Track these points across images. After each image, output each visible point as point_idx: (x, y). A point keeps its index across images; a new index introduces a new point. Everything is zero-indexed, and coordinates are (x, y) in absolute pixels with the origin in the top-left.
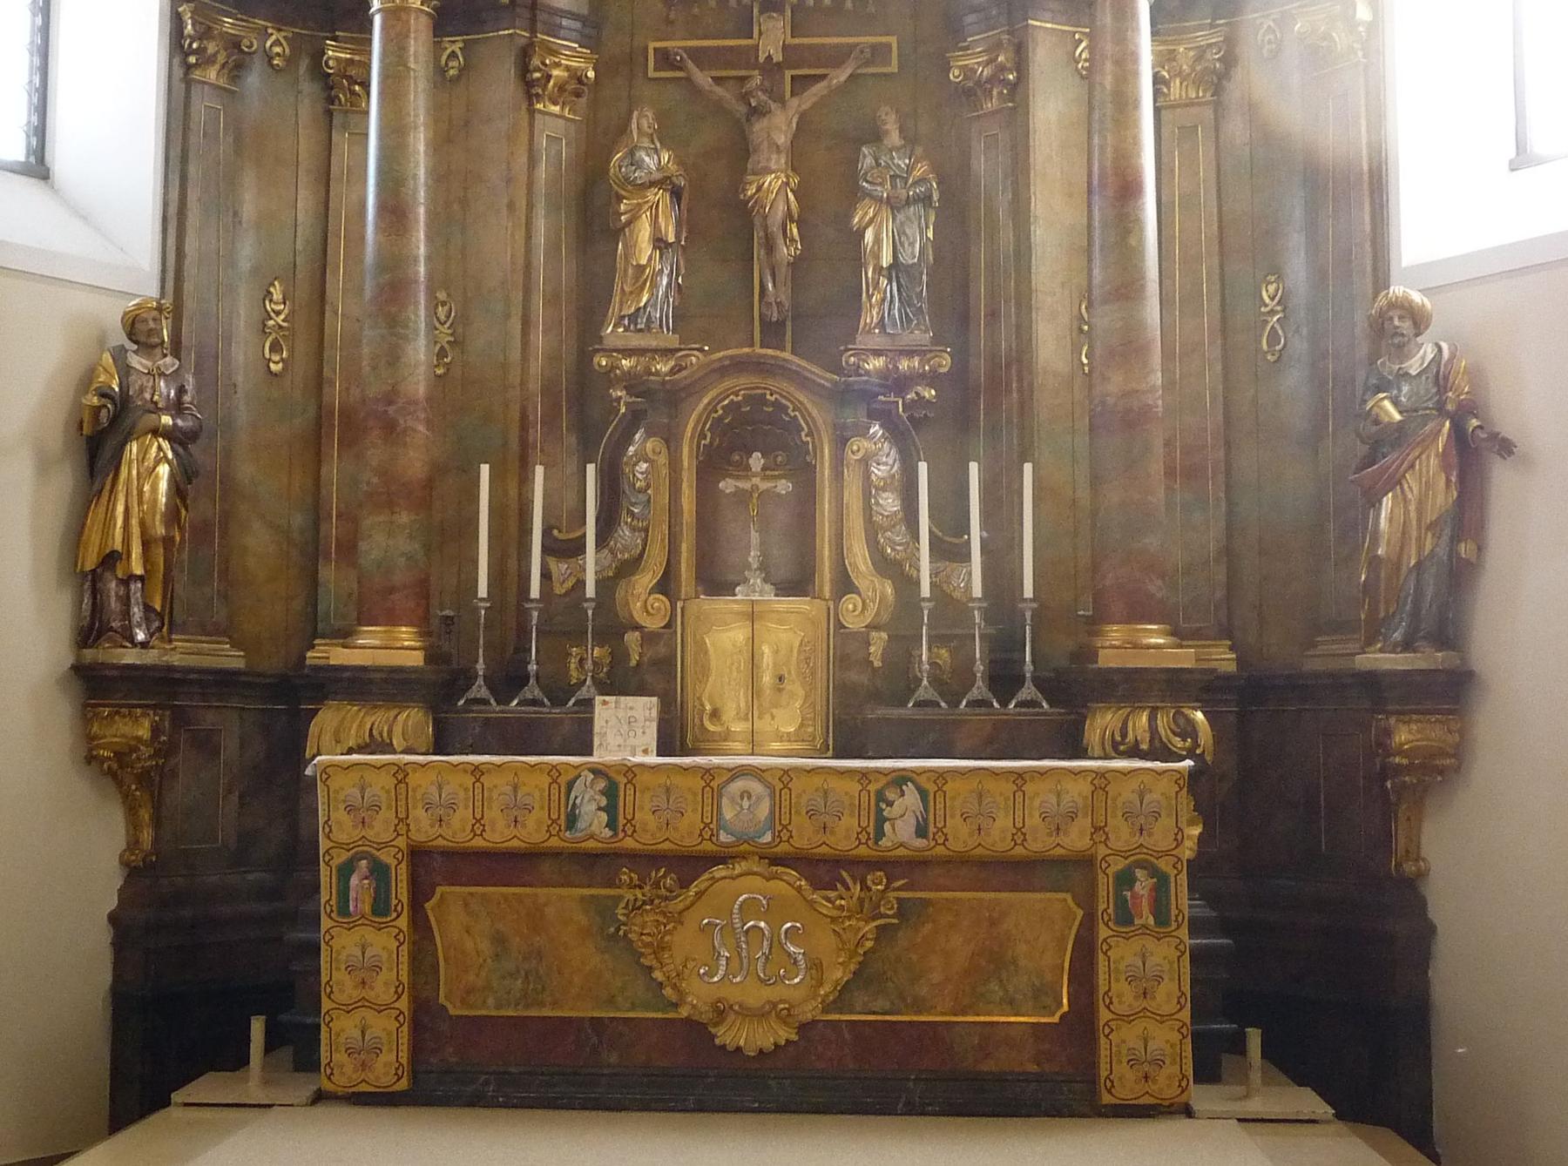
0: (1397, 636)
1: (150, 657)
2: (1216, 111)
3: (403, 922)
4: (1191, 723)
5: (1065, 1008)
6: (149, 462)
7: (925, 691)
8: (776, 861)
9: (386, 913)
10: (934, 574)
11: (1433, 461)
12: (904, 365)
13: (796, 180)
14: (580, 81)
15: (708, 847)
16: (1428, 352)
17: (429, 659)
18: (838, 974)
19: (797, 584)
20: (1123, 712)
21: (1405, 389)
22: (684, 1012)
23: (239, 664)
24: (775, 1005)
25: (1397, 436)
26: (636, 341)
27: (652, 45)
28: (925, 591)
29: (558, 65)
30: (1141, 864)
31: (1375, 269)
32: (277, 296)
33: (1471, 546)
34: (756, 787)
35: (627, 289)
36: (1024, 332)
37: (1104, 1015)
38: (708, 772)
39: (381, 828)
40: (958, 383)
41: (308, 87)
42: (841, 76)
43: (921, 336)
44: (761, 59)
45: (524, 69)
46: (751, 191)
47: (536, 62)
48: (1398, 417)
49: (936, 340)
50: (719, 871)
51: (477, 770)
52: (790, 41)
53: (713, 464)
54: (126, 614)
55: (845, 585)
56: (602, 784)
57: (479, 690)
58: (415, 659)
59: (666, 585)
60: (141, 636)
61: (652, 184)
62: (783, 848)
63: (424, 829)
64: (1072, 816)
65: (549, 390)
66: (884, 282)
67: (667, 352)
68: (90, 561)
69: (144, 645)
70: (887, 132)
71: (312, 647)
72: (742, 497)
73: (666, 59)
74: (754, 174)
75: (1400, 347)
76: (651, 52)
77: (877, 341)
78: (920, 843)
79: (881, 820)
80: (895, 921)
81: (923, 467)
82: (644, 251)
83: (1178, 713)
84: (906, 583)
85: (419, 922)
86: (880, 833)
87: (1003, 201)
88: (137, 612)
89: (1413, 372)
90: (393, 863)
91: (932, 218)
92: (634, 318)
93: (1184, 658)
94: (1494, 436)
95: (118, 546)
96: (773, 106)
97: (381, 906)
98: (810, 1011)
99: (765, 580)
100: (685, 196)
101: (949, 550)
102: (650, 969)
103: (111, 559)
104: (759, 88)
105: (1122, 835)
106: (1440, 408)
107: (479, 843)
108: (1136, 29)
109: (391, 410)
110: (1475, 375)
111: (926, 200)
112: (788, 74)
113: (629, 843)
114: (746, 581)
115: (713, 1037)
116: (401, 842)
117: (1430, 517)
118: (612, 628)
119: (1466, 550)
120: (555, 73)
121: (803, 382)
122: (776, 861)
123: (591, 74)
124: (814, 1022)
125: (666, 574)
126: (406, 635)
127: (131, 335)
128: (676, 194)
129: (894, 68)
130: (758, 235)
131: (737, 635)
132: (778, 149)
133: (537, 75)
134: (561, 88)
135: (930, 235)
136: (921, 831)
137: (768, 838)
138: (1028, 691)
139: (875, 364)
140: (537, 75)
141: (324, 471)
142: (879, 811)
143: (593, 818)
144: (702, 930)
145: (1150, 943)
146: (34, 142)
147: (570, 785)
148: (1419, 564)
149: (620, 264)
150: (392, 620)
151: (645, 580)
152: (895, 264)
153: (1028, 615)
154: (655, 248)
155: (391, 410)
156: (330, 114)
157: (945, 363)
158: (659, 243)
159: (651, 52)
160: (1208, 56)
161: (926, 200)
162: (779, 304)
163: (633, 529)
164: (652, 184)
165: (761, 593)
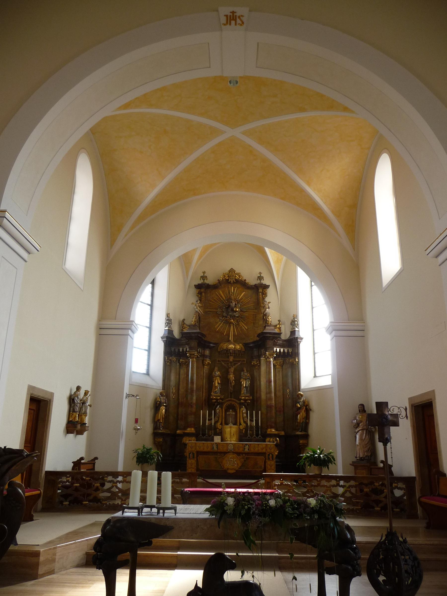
0: (300, 430)
1: (162, 431)
2: (282, 369)
3: (196, 459)
4: (277, 440)
5: (263, 469)
6: (163, 409)
7: (249, 436)
8: (234, 453)
9: (194, 458)
10: (250, 423)
11: (303, 411)
12: (246, 398)
13: (234, 376)
14: (209, 364)
15: (227, 451)
16: (303, 399)
17: (196, 432)
18: (240, 465)
19: (235, 424)
20: (270, 438)
21: (301, 403)
22: (224, 469)
23: (170, 433)
24: (233, 468)
25: (300, 408)
26: (216, 395)
27: (217, 359)
28: (249, 425)
29: (206, 362)
30: (270, 453)
31: (299, 389)
32: (174, 389)
33: (308, 421)
34: (232, 445)
35: (215, 388)
36: (260, 394)
37: (267, 469)
38: (227, 443)
39: (193, 449)
40: (253, 401)
41: (178, 364)
42: (239, 363)
43: (248, 395)
44: (230, 361)
45: (203, 363)
46: (229, 377)
47: (204, 362)
48: (299, 406)
49: (250, 395)
50: (228, 454)
51: (203, 443)
52: (233, 359)
53: (226, 411)
54: (160, 426)
55: (240, 424)
56: (216, 445)
57: (201, 435)
58: (194, 432)
59: (221, 424)
60: (161, 429)
61: (217, 376)
62: (235, 451)
63: (198, 449)
64: (264, 448)
65: (205, 400)
66: (244, 388)
67: (219, 396)
68: (156, 420)
69: (162, 430)
70: (245, 370)
71: (177, 431)
72: (229, 414)
73: (219, 361)
74: (229, 375)
75: (300, 398)
76: (217, 360)
77: (243, 395)
78: (248, 451)
79: (244, 449)
80: (246, 459)
81: (249, 411)
82: (217, 384)
83: (276, 438)
84: (247, 424)
85: (197, 460)
86: (244, 450)
87: (258, 378)
88: (161, 426)
89: (301, 401)
90: (195, 453)
91: (250, 381)
92: (215, 392)
93: (277, 432)
94: (309, 409)
95: (159, 419)
96: (231, 367)
97: (193, 457)
98: (237, 469)
99: (232, 424)
100: (221, 377)
101: (251, 420)
102: (221, 464)
103: (159, 420)
104: (230, 365)
105: (269, 450)
106: (304, 405)
107: (204, 451)
108: (271, 365)
109: (192, 404)
110: (308, 402)
111: (249, 378)
112: (233, 363)
113: (219, 451)
114: (230, 424)
115: (227, 472)
116: (196, 451)
117: (303, 417)
118: (215, 428)
119: (307, 421)
120: (206, 363)
121: (236, 402)
122: (234, 453)
123: (210, 363)
124: (238, 470)
125: (222, 422)
126: (193, 429)
127: (161, 395)
128: (220, 377)
129: (245, 363)
130: (230, 382)
131: (229, 429)
132: (232, 372)
133: (204, 363)
134: (207, 364)
135: (250, 382)
136: (248, 450)
137: (233, 450)
138: (260, 436)
139: (243, 398)
140: (204, 363)
141: (179, 409)
142: (244, 448)
143: (215, 448)
144: (226, 460)
145: (271, 462)
146: (148, 371)
147: (213, 445)
148: (302, 422)
149: (213, 385)
150: (191, 427)
151: (219, 423)
152: (245, 386)
153: (260, 428)
154: (218, 384)
155: (192, 404)
156: (180, 367)
157: (251, 398)
158: (218, 383)
159: (217, 360)
160: (281, 363)
161: (249, 378)
162: (232, 390)
163: (217, 417)
164: (217, 376)
165: (232, 425)
